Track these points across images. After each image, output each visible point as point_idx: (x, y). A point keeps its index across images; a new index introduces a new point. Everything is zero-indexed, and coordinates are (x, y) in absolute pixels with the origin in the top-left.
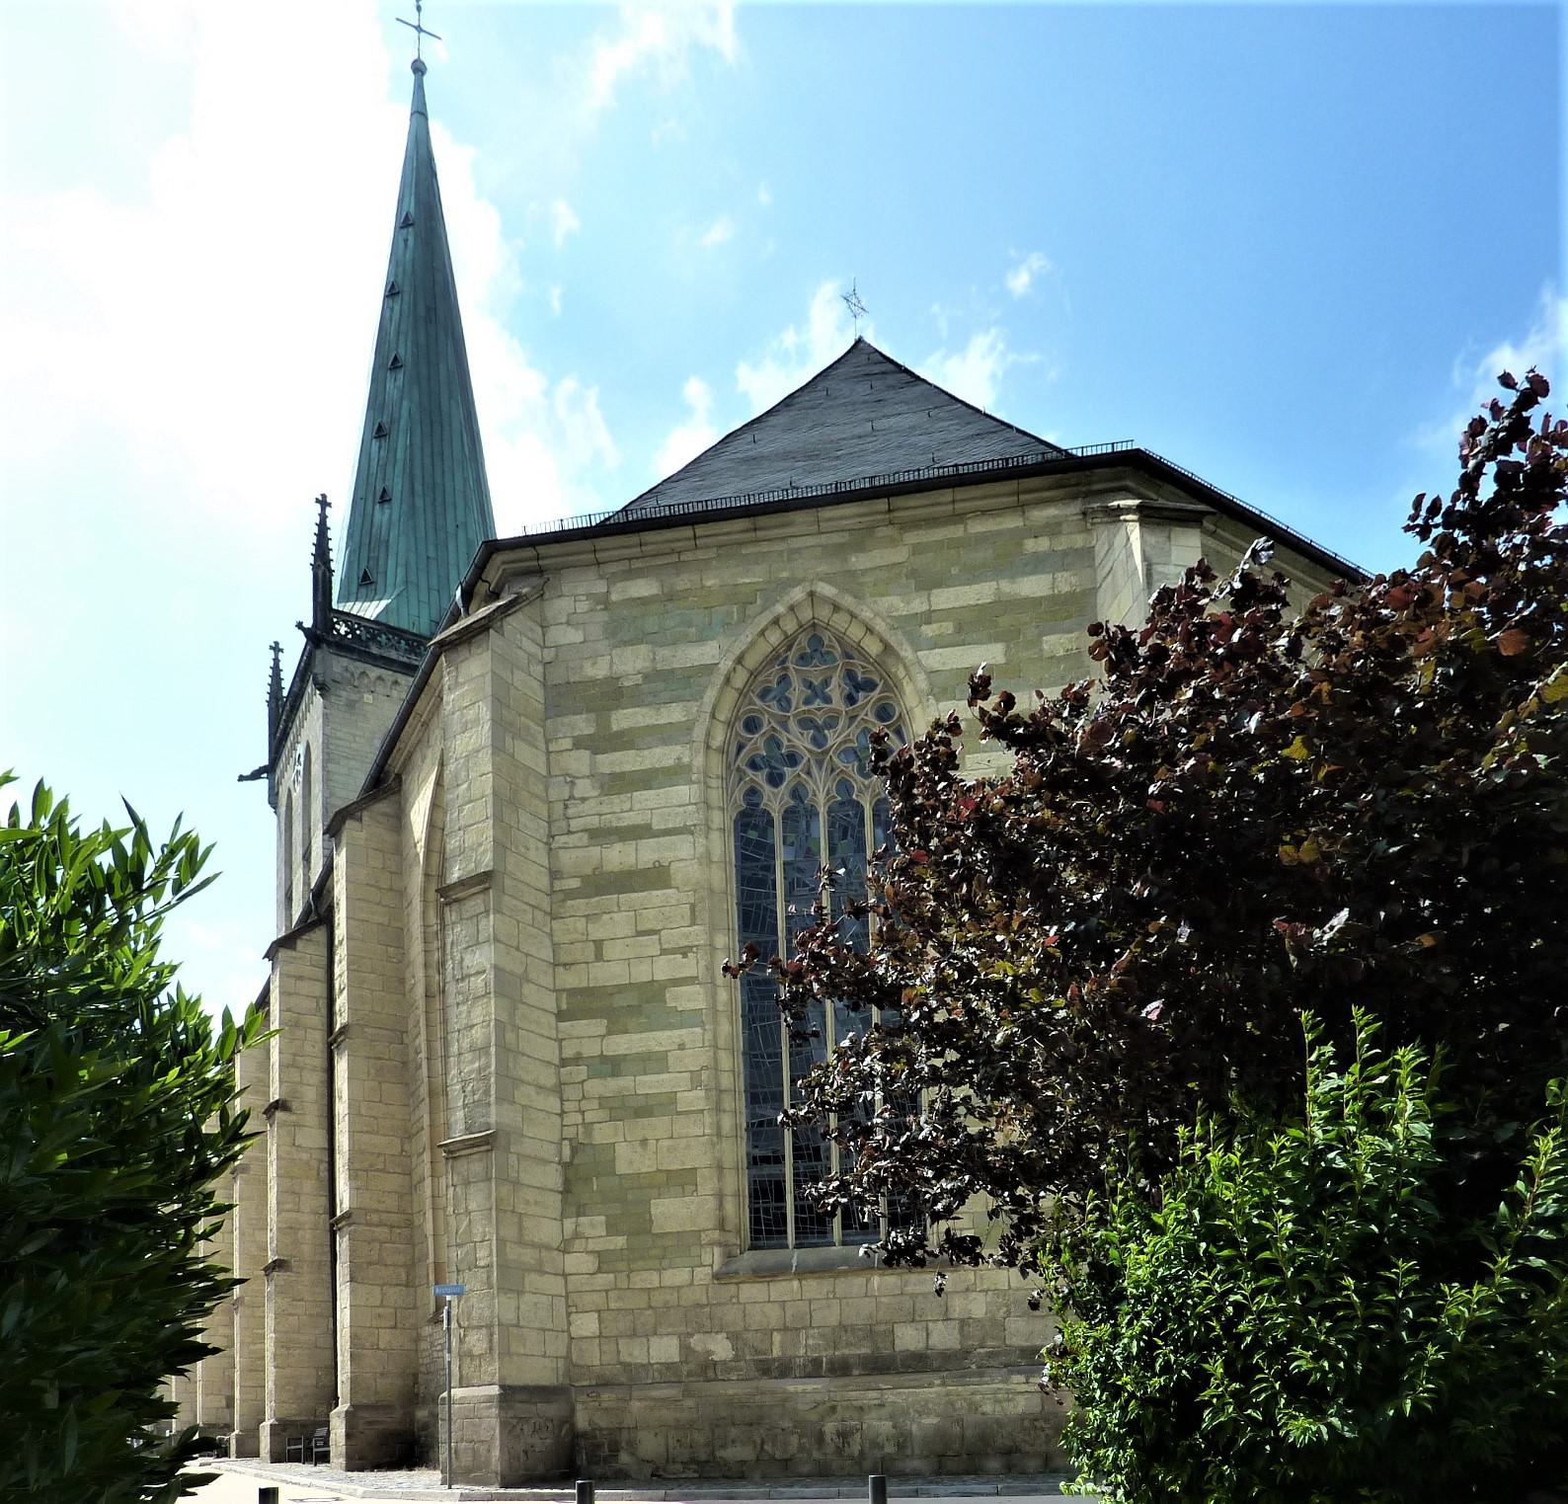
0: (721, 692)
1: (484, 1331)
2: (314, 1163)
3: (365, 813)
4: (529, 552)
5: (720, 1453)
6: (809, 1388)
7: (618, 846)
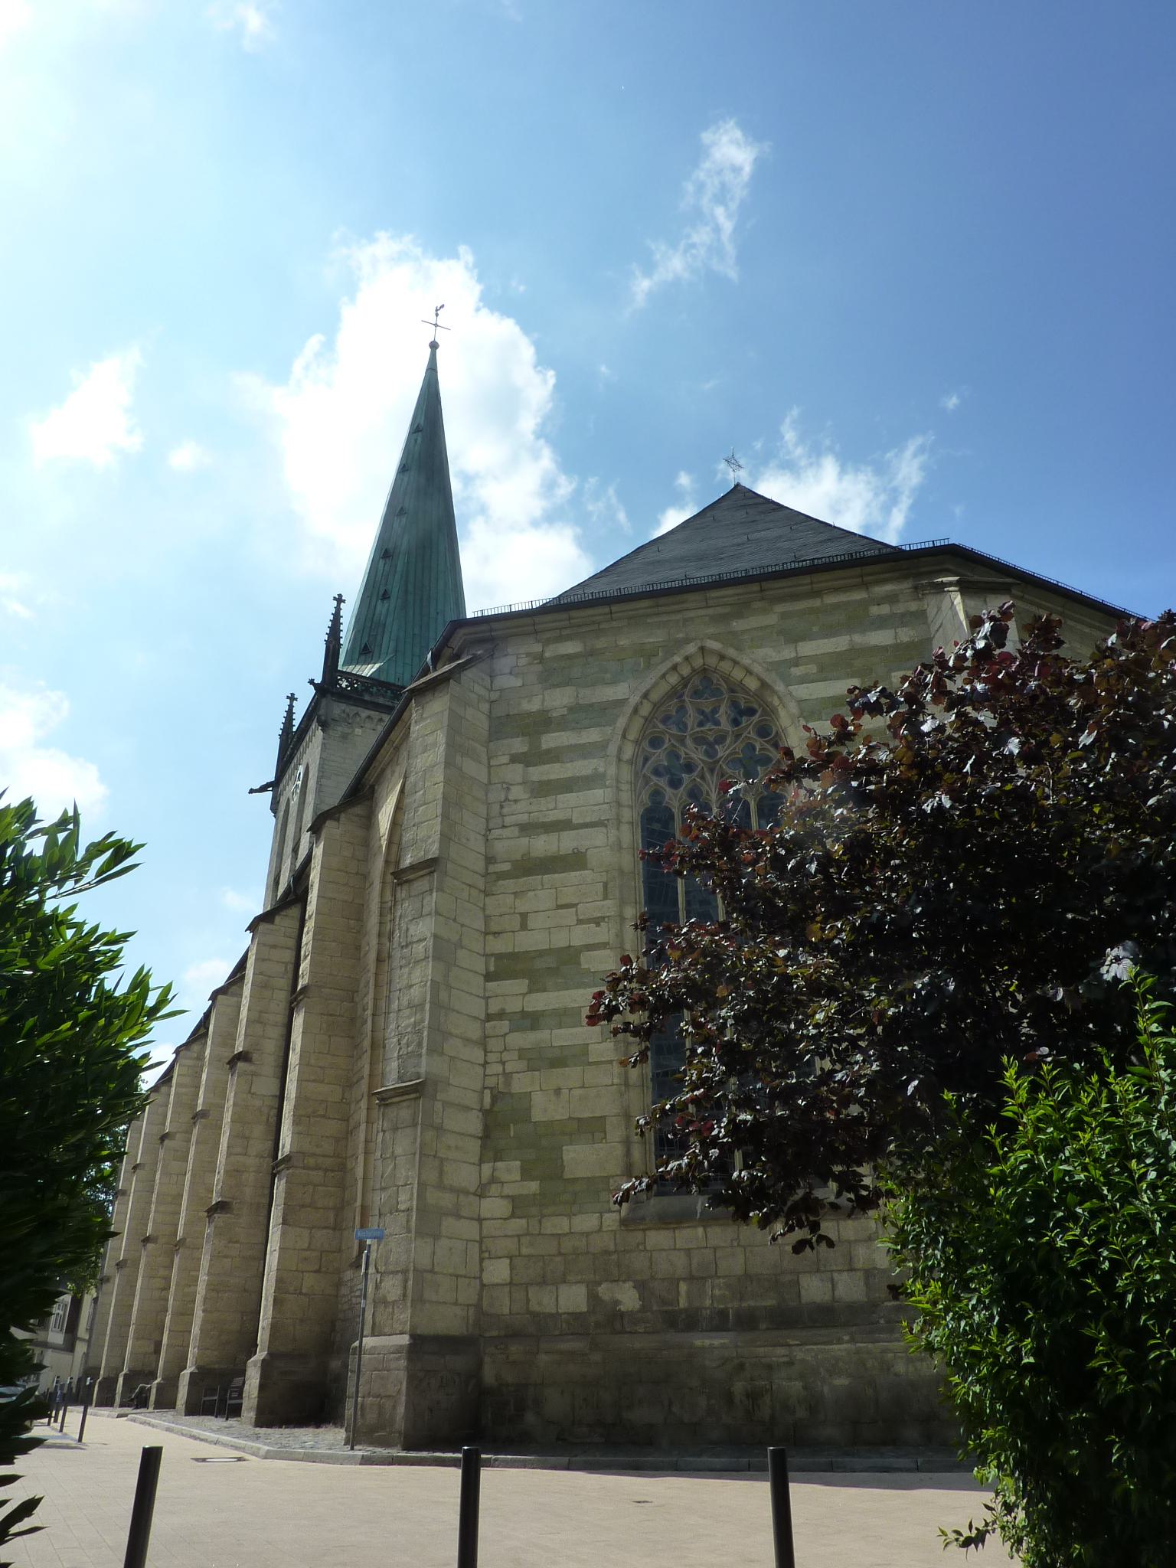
2: (265, 1110)
6: (717, 1342)
7: (543, 837)
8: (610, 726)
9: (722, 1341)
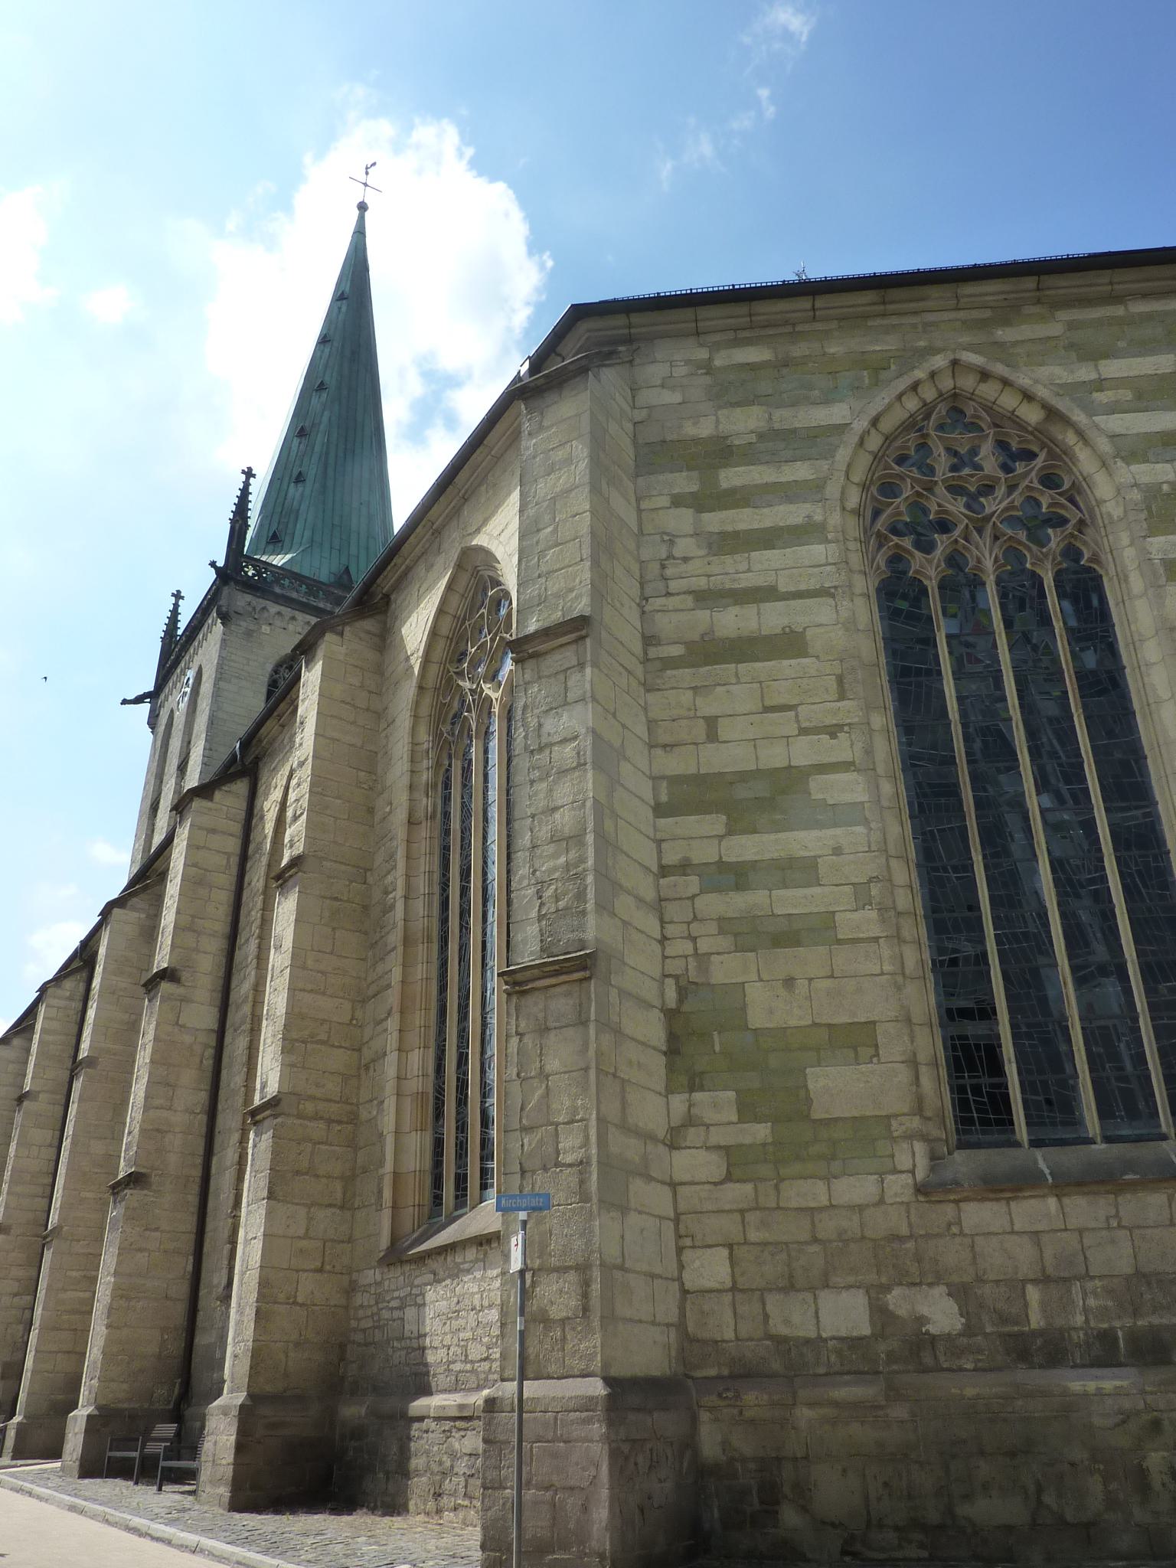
0: (855, 454)
1: (572, 1276)
3: (347, 629)
4: (620, 320)
5: (964, 1510)
6: (1108, 1385)
7: (734, 610)
8: (826, 458)
9: (1118, 1383)
